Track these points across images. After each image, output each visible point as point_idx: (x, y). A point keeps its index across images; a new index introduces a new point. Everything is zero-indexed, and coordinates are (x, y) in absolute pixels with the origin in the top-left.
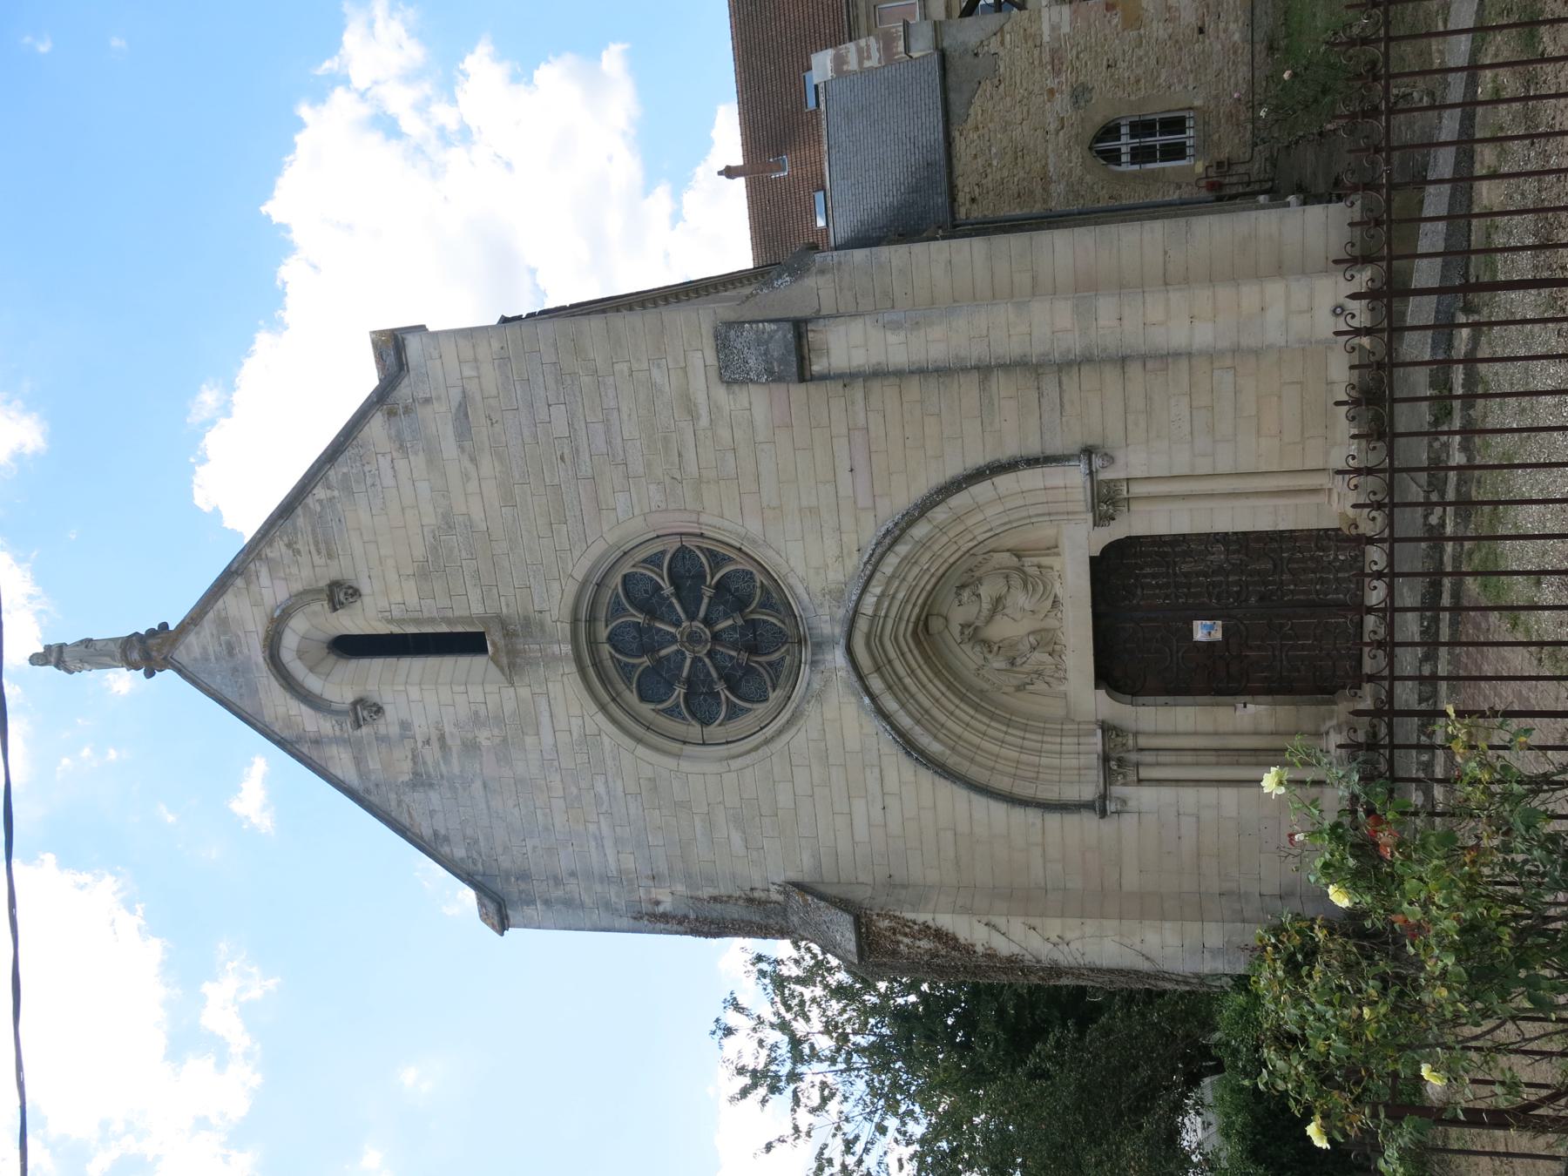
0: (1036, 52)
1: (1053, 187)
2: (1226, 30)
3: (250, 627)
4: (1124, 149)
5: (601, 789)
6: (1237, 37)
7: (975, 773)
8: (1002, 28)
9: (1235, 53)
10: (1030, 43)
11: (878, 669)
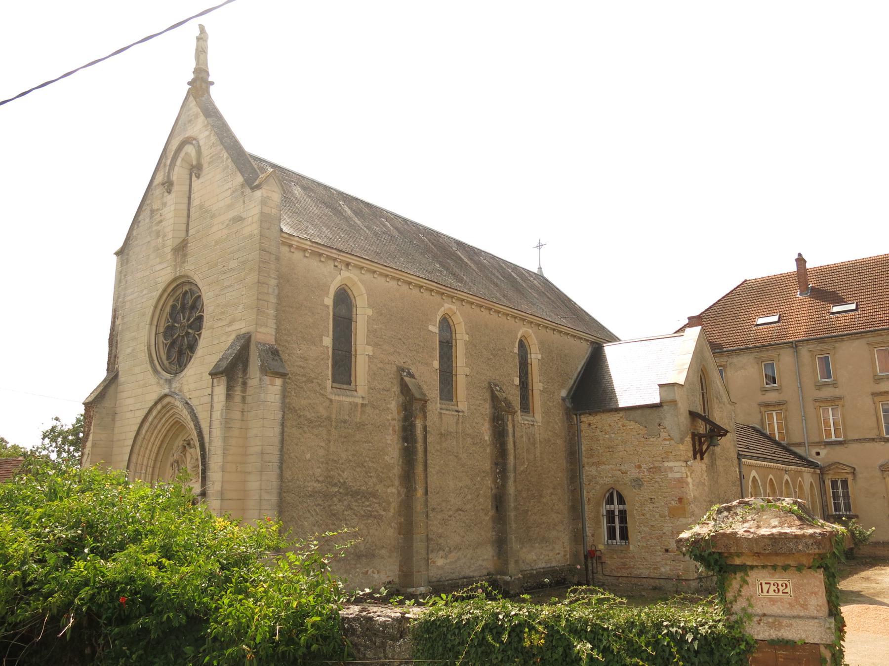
0: (660, 459)
1: (594, 468)
2: (666, 564)
3: (195, 129)
4: (612, 506)
5: (145, 292)
6: (663, 570)
7: (137, 447)
8: (672, 439)
9: (655, 568)
10: (664, 455)
11: (163, 407)
